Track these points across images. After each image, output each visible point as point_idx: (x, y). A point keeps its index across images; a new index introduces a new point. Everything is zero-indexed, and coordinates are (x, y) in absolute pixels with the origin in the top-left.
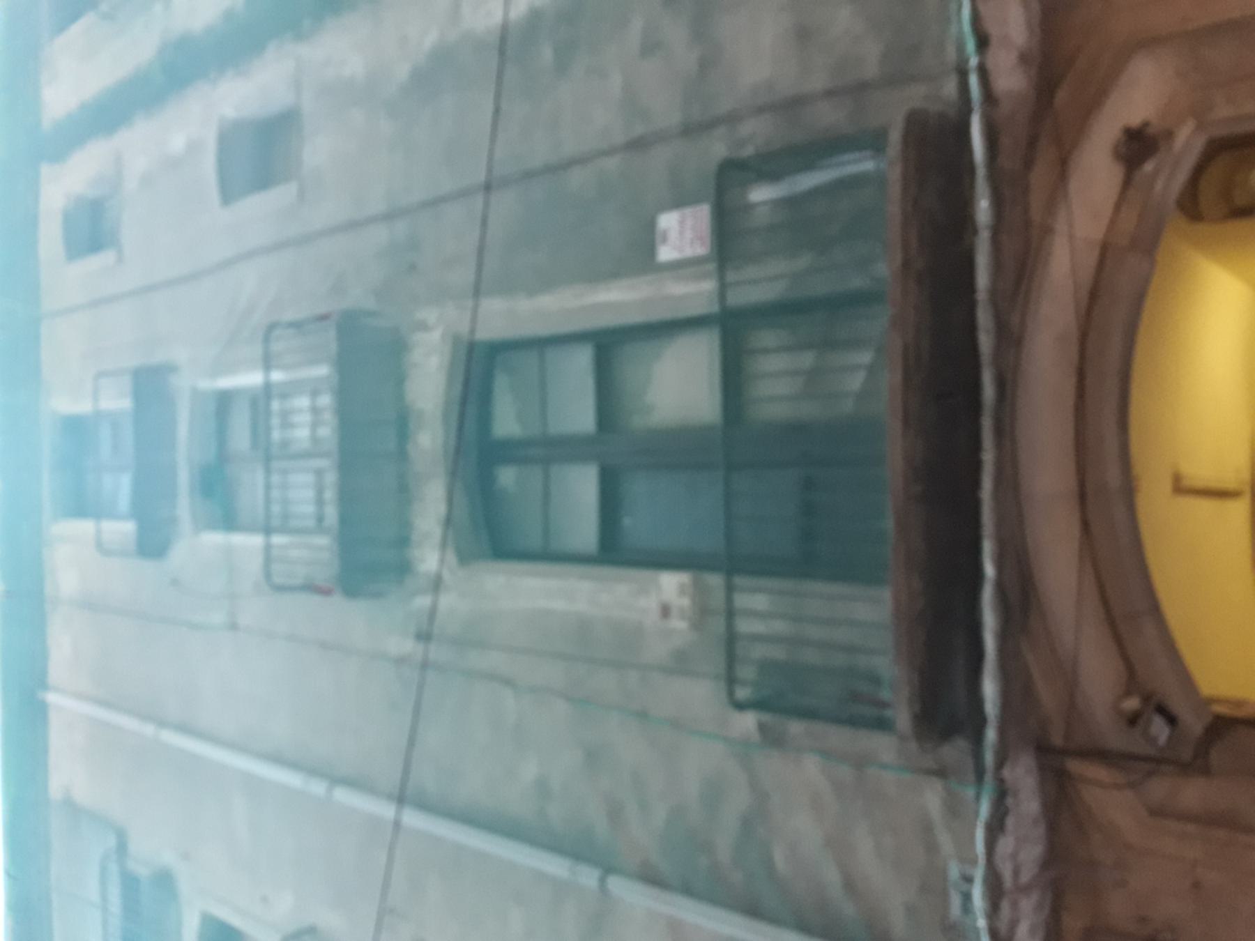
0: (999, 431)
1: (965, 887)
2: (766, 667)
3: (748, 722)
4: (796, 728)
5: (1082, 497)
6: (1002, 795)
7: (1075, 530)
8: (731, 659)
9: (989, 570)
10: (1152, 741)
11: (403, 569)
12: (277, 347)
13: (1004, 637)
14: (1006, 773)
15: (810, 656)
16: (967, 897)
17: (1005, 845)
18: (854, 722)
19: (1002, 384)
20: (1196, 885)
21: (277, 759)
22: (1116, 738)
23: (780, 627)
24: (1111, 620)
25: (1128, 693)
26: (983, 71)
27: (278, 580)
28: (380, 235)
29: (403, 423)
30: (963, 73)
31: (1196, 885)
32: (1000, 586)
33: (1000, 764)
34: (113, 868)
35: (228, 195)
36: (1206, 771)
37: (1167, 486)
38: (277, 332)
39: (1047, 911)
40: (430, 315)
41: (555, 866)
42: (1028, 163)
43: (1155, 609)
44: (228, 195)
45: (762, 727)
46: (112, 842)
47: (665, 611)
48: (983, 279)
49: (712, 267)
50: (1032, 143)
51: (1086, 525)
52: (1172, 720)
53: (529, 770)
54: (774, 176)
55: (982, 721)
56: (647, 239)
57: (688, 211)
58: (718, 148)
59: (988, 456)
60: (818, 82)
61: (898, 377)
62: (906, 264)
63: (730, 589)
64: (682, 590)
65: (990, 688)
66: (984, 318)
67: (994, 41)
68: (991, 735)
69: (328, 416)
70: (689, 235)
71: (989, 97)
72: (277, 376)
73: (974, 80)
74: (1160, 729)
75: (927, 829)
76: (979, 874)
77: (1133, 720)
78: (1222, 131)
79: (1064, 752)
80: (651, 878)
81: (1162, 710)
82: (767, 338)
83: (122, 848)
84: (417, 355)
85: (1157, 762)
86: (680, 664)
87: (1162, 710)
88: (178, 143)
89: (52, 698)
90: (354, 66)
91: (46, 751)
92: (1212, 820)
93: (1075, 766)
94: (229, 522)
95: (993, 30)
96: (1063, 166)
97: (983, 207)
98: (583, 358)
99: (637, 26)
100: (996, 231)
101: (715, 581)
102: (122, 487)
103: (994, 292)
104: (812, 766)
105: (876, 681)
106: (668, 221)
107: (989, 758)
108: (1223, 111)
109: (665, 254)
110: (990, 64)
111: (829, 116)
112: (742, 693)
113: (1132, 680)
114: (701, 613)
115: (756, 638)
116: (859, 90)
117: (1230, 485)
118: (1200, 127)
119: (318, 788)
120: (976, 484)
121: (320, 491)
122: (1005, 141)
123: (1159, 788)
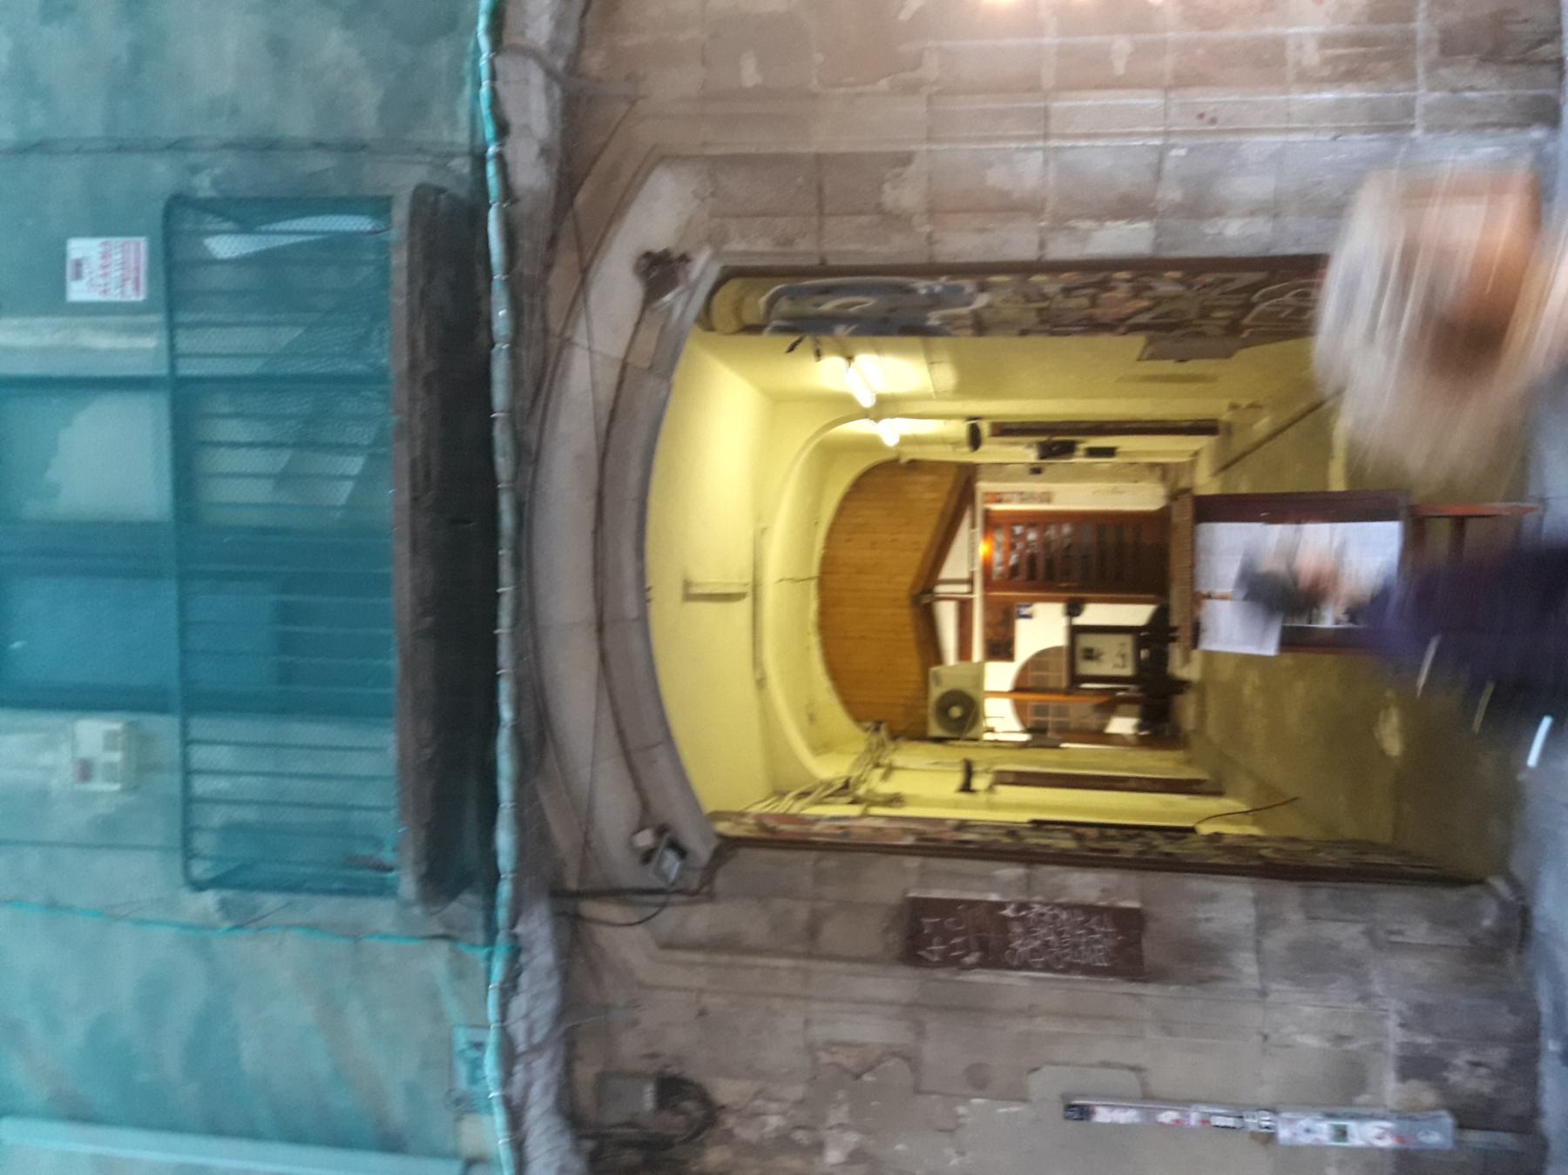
0: (517, 563)
1: (473, 1054)
2: (231, 830)
3: (209, 899)
5: (600, 629)
6: (516, 951)
8: (188, 831)
9: (506, 713)
10: (664, 876)
13: (522, 781)
14: (519, 929)
15: (296, 817)
16: (476, 1065)
17: (519, 1005)
20: (702, 1013)
22: (628, 873)
24: (626, 753)
25: (641, 828)
26: (500, 158)
30: (479, 160)
31: (702, 1013)
32: (518, 730)
33: (514, 920)
36: (711, 897)
37: (678, 593)
39: (557, 1068)
42: (548, 267)
43: (668, 739)
45: (224, 905)
47: (85, 770)
49: (157, 318)
50: (553, 242)
51: (603, 658)
52: (682, 853)
54: (246, 227)
55: (495, 877)
57: (116, 241)
58: (162, 174)
59: (506, 590)
61: (406, 497)
62: (413, 366)
63: (187, 742)
64: (110, 742)
65: (504, 840)
66: (501, 437)
67: (514, 130)
68: (505, 890)
70: (116, 274)
71: (508, 192)
73: (491, 169)
74: (671, 863)
75: (433, 996)
76: (492, 1038)
77: (647, 856)
79: (579, 895)
80: (79, 1114)
82: (220, 403)
96: (584, 272)
97: (501, 315)
100: (514, 343)
101: (164, 727)
103: (511, 411)
105: (379, 844)
106: (79, 248)
108: (736, 245)
109: (78, 292)
110: (509, 157)
112: (200, 870)
113: (646, 816)
114: (140, 769)
115: (217, 800)
116: (352, 148)
118: (716, 256)
120: (493, 621)
122: (525, 244)
123: (670, 919)
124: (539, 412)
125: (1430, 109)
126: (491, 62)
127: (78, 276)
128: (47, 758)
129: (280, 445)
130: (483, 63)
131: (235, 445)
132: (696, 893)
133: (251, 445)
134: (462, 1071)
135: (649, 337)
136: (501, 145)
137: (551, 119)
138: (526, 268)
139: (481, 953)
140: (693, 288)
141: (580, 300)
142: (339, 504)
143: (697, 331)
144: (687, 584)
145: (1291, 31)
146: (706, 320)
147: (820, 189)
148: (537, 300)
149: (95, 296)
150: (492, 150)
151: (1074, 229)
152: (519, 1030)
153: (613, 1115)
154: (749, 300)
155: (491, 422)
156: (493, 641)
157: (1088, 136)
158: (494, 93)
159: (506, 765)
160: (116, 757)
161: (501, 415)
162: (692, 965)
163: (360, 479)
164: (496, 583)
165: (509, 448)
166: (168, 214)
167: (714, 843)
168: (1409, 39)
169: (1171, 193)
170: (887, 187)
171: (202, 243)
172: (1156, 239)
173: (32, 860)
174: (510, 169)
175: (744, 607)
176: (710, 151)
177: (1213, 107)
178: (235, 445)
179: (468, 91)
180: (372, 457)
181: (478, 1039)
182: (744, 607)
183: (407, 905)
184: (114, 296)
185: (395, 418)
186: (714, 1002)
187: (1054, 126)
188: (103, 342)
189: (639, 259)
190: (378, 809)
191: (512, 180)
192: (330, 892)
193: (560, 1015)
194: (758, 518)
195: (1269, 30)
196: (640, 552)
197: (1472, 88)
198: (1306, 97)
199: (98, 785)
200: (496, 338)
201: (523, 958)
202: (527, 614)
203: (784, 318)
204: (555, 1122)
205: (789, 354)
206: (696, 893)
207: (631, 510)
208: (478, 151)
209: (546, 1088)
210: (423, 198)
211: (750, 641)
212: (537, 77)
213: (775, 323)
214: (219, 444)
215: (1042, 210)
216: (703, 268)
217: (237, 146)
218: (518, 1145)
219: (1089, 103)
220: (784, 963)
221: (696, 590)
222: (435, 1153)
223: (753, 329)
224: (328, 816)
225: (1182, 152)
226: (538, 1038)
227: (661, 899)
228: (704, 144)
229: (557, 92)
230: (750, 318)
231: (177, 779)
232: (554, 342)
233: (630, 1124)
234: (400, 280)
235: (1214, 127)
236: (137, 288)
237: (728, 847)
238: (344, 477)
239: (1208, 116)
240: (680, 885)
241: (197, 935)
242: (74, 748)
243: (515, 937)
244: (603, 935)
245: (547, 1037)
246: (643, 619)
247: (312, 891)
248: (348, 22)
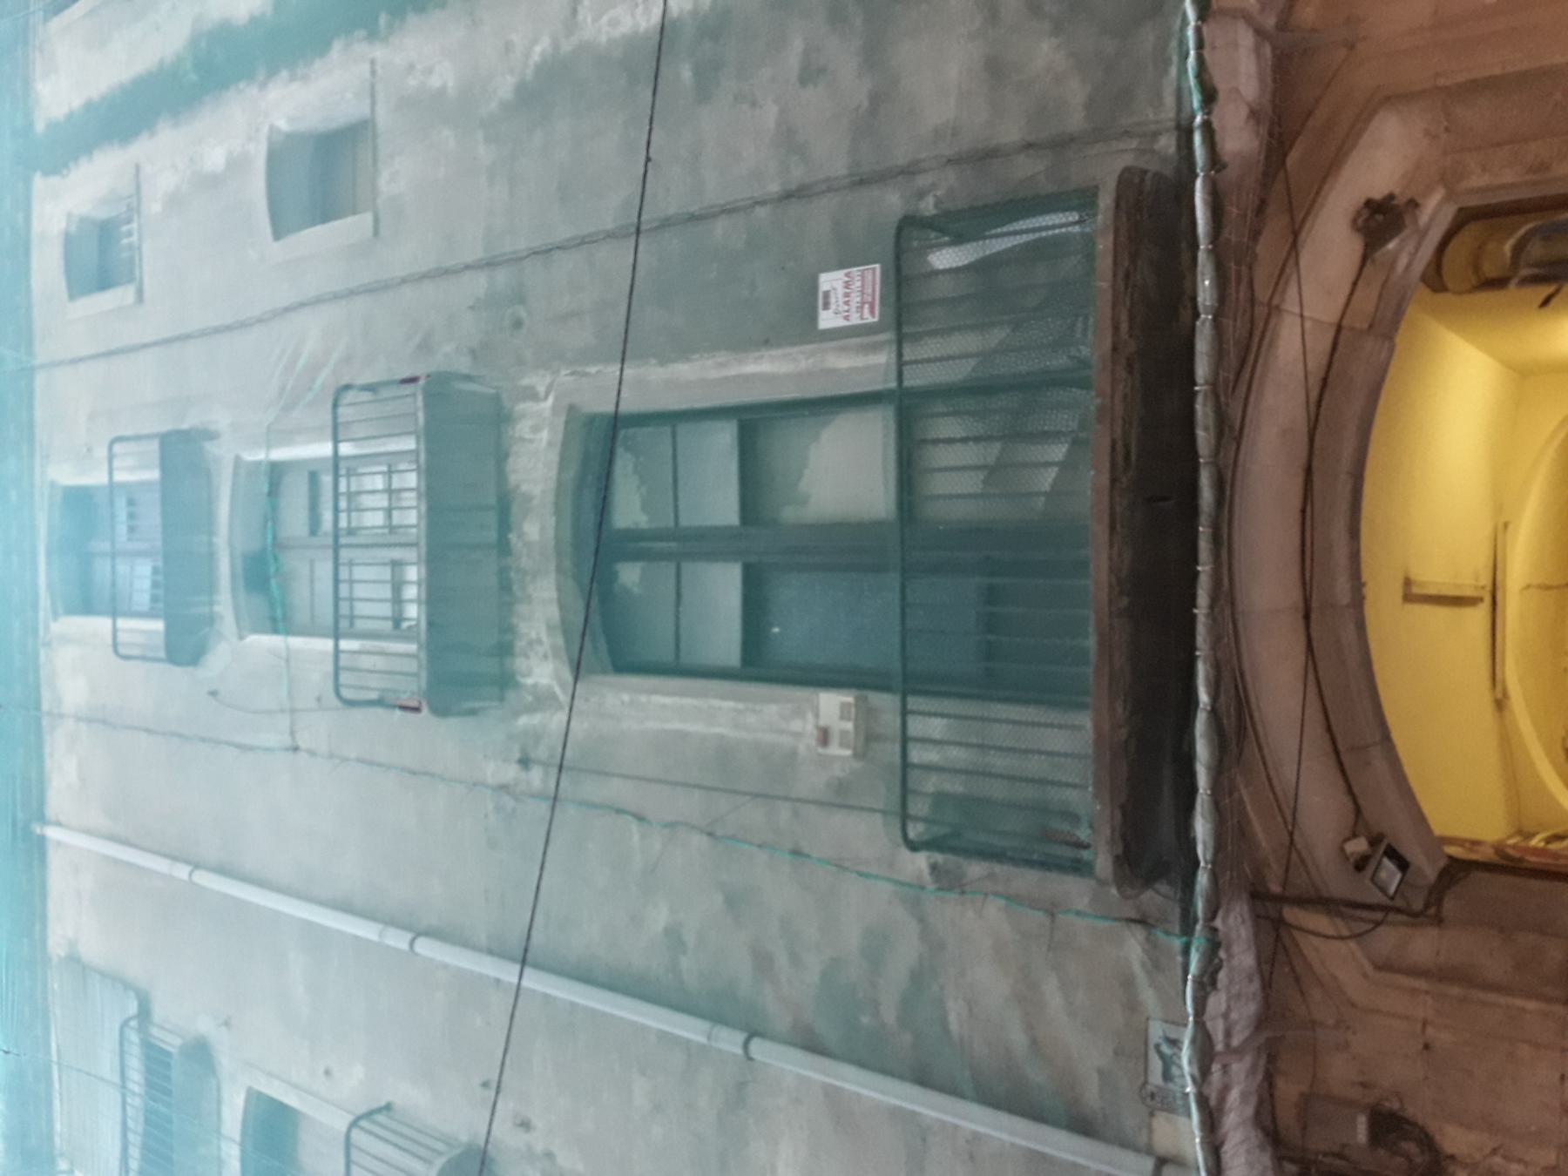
0: (1216, 539)
2: (940, 799)
3: (920, 862)
4: (975, 869)
6: (1214, 945)
7: (1300, 647)
9: (1204, 697)
11: (505, 682)
12: (345, 413)
13: (1219, 771)
14: (1218, 923)
15: (998, 791)
16: (1168, 1064)
17: (1216, 1003)
18: (1046, 864)
19: (1220, 485)
20: (1427, 1047)
21: (345, 907)
22: (1339, 884)
23: (957, 755)
26: (1207, 127)
27: (347, 693)
28: (479, 284)
29: (505, 508)
30: (1185, 133)
32: (1214, 712)
33: (1212, 914)
34: (134, 1037)
35: (280, 230)
36: (1439, 921)
38: (350, 396)
40: (540, 381)
41: (690, 1029)
42: (1255, 235)
44: (280, 230)
45: (934, 868)
46: (133, 1008)
47: (824, 736)
48: (1202, 369)
49: (889, 336)
50: (1261, 208)
52: (1403, 865)
53: (659, 917)
54: (959, 239)
56: (808, 301)
57: (855, 270)
58: (893, 202)
59: (1204, 569)
60: (1011, 132)
61: (1105, 479)
63: (905, 713)
65: (1202, 828)
66: (1203, 410)
67: (1222, 96)
68: (1203, 879)
69: (410, 499)
70: (856, 299)
71: (1215, 160)
72: (346, 449)
73: (1197, 138)
74: (1390, 874)
75: (1128, 983)
77: (1361, 864)
78: (1474, 201)
79: (1281, 899)
80: (813, 1045)
81: (1393, 854)
83: (144, 1014)
84: (523, 428)
85: (1387, 910)
86: (841, 797)
87: (1393, 854)
88: (215, 158)
89: (52, 833)
90: (445, 76)
91: (44, 897)
92: (1443, 974)
93: (1292, 914)
94: (279, 621)
95: (1222, 85)
97: (1205, 285)
98: (724, 437)
99: (797, 45)
101: (886, 702)
102: (140, 577)
103: (1214, 384)
104: (994, 909)
105: (1075, 819)
106: (831, 281)
107: (1200, 906)
108: (1477, 180)
110: (1216, 125)
111: (1028, 168)
112: (915, 830)
113: (1358, 821)
114: (867, 738)
115: (929, 768)
116: (1061, 144)
117: (1469, 592)
118: (1450, 196)
119: (398, 940)
120: (1192, 601)
121: (397, 586)
123: (1388, 939)
124: (1242, 389)
126: (1198, 30)
127: (826, 306)
128: (796, 725)
129: (989, 438)
130: (1190, 33)
131: (950, 441)
132: (1416, 915)
133: (964, 440)
134: (1156, 1065)
135: (1367, 299)
136: (1209, 113)
137: (1262, 80)
138: (1231, 234)
139: (1177, 943)
140: (1423, 234)
141: (1291, 262)
142: (1043, 489)
143: (1424, 293)
144: (1408, 582)
146: (1435, 279)
148: (1244, 269)
149: (840, 322)
150: (1198, 119)
152: (1217, 1030)
153: (1320, 1141)
154: (1491, 246)
155: (1194, 395)
156: (1192, 619)
158: (1200, 60)
159: (1203, 750)
160: (849, 726)
161: (1204, 388)
162: (1414, 992)
163: (1064, 466)
164: (1194, 560)
165: (1211, 421)
166: (900, 230)
167: (1442, 863)
171: (926, 262)
173: (784, 812)
174: (1218, 138)
175: (1480, 614)
176: (1442, 82)
178: (950, 441)
179: (1173, 71)
180: (1076, 442)
181: (1173, 1036)
182: (1477, 618)
183: (1102, 883)
184: (855, 320)
185: (1098, 401)
186: (1442, 1037)
188: (843, 362)
189: (1359, 213)
190: (1074, 786)
191: (1219, 146)
192: (1029, 863)
193: (1262, 1021)
194: (1498, 508)
196: (1354, 533)
199: (835, 750)
200: (1201, 308)
201: (1222, 954)
202: (1225, 595)
203: (1537, 265)
204: (1255, 1136)
205: (1543, 310)
206: (1416, 915)
207: (1344, 487)
208: (1184, 123)
209: (1244, 1097)
210: (1129, 182)
212: (1246, 38)
213: (1525, 272)
214: (936, 441)
216: (1435, 212)
217: (953, 161)
218: (1214, 1148)
220: (1532, 1005)
221: (1415, 590)
222: (1125, 1144)
223: (1498, 283)
224: (1029, 793)
226: (1235, 1042)
227: (1378, 916)
228: (1437, 75)
229: (1267, 50)
230: (1490, 270)
231: (897, 748)
232: (1260, 311)
233: (1340, 1156)
234: (1105, 263)
236: (872, 312)
237: (1456, 871)
238: (1047, 464)
240: (1399, 903)
241: (911, 894)
242: (817, 716)
243: (1215, 930)
244: (1313, 949)
245: (1246, 1041)
246: (1358, 601)
247: (1013, 861)
248: (1057, 28)
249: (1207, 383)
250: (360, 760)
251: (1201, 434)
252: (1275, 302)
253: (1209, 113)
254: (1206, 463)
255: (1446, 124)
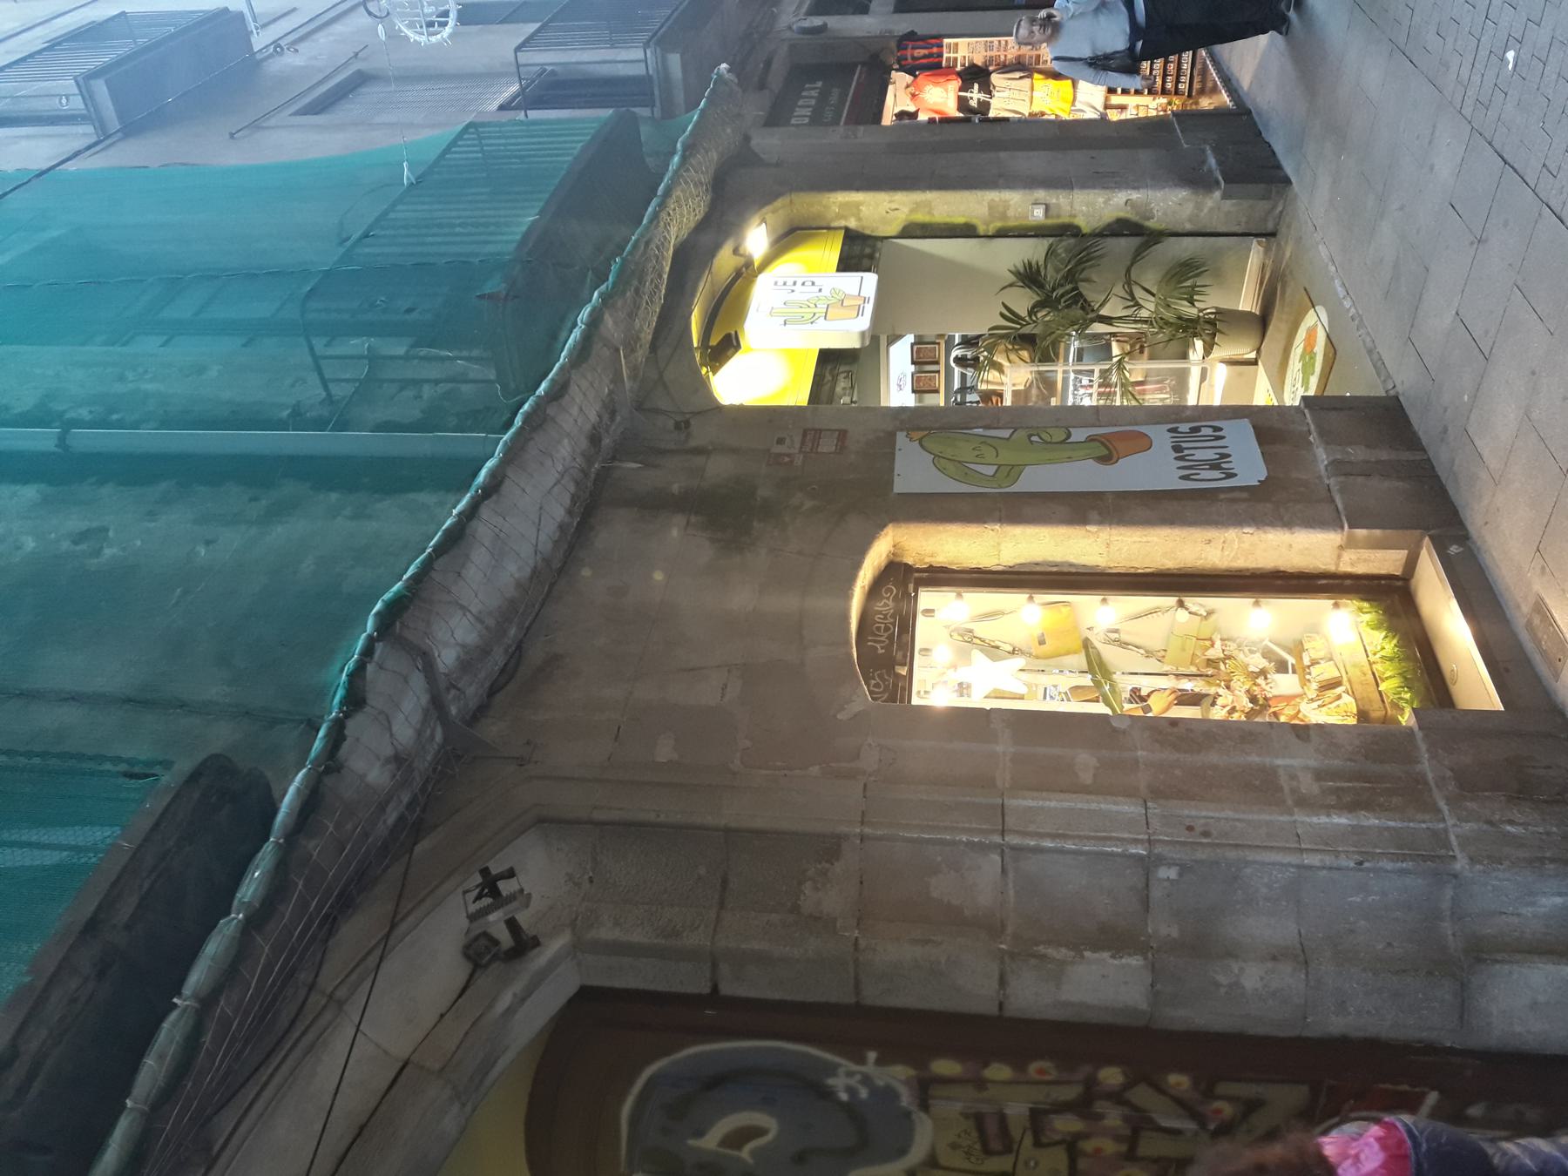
48: (198, 977)
93: (1071, 429)
125: (1464, 841)
126: (371, 641)
145: (1279, 762)
147: (725, 882)
151: (1043, 957)
157: (1053, 836)
158: (361, 667)
168: (1421, 780)
169: (1164, 928)
170: (807, 887)
172: (1152, 986)
177: (1202, 821)
181: (797, 283)
187: (1011, 821)
195: (1255, 759)
197: (1511, 822)
198: (1315, 820)
211: (462, 986)
215: (1003, 926)
219: (1053, 804)
225: (1172, 873)
235: (1205, 840)
239: (1198, 829)
249: (195, 996)
250: (1380, 692)
251: (150, 1062)
252: (341, 993)
253: (347, 715)
254: (132, 1109)
255: (591, 874)
